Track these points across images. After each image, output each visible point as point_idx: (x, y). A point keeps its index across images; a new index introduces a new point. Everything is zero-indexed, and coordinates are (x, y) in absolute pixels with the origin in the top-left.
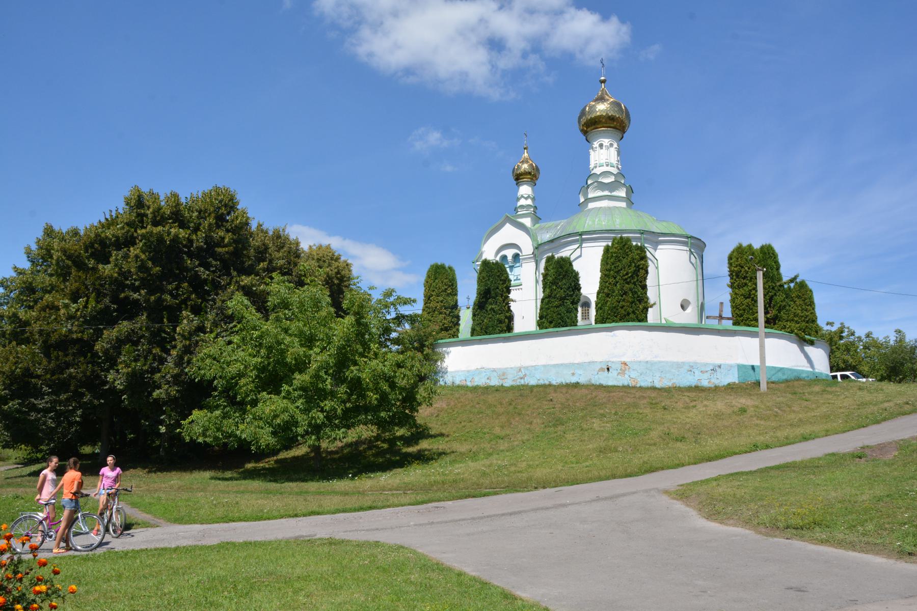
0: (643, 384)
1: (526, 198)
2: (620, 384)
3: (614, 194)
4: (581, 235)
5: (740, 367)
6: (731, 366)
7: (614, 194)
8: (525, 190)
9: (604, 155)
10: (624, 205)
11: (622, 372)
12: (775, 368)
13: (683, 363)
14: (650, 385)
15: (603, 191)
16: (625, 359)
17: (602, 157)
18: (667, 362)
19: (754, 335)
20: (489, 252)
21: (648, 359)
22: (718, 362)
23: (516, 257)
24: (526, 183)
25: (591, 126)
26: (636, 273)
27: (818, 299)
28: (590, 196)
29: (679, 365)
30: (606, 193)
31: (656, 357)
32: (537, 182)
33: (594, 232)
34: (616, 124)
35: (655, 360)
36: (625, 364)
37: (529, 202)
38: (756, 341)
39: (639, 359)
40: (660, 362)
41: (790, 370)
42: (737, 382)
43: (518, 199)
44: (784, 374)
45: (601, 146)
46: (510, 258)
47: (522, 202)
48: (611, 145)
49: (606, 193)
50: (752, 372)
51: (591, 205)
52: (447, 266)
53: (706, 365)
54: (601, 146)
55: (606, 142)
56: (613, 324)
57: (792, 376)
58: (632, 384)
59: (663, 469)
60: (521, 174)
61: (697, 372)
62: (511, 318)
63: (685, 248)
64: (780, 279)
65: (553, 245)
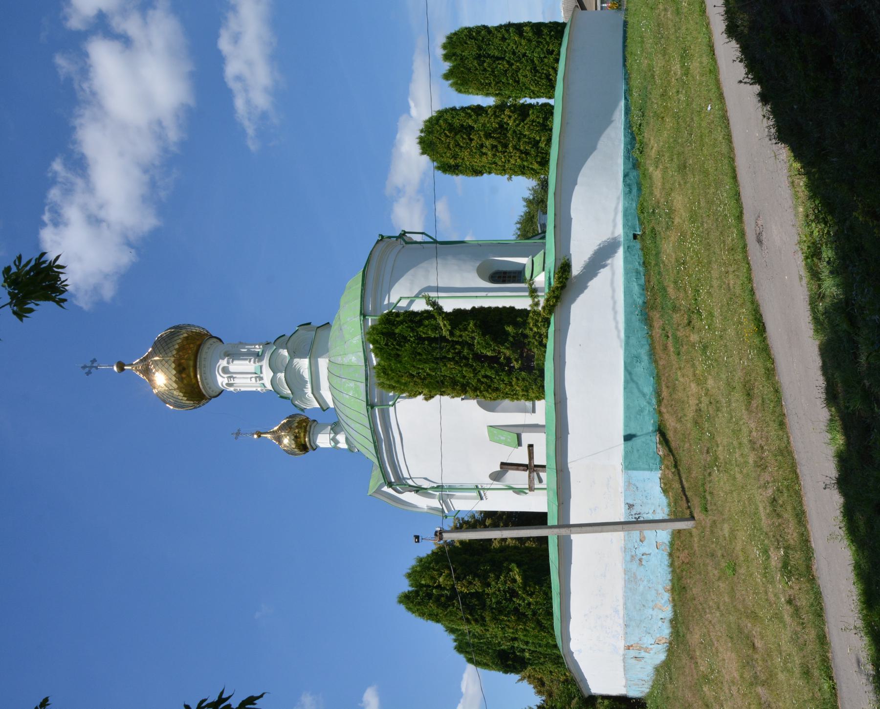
3: (306, 375)
5: (630, 464)
6: (629, 484)
7: (306, 375)
12: (626, 382)
13: (626, 572)
18: (626, 598)
19: (565, 547)
26: (471, 37)
27: (470, 21)
29: (631, 580)
30: (308, 390)
31: (617, 611)
35: (621, 613)
38: (578, 540)
40: (626, 607)
41: (627, 344)
42: (659, 474)
44: (637, 358)
48: (225, 370)
49: (308, 390)
50: (636, 442)
57: (641, 330)
59: (752, 292)
61: (643, 549)
62: (556, 24)
63: (391, 409)
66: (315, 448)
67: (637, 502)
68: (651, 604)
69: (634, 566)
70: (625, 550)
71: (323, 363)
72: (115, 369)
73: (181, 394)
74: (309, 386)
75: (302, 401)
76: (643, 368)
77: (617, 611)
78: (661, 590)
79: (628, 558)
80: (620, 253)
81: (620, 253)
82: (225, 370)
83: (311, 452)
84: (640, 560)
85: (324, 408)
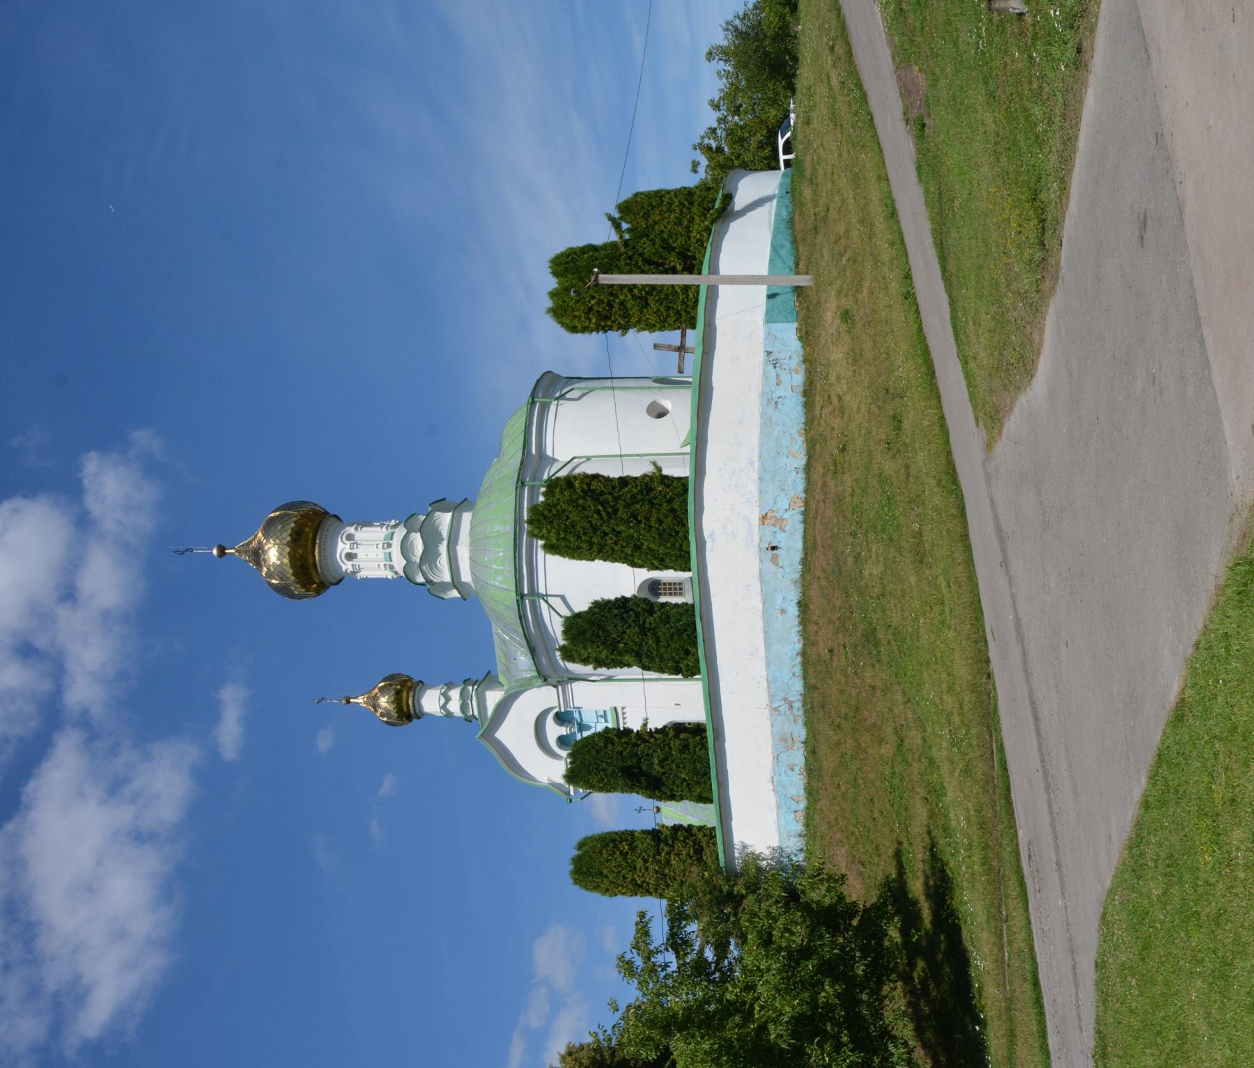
1: (448, 699)
2: (800, 527)
3: (445, 532)
5: (770, 318)
6: (768, 335)
7: (445, 532)
8: (430, 702)
11: (779, 523)
13: (762, 416)
14: (802, 475)
16: (755, 519)
18: (761, 445)
21: (755, 477)
22: (761, 357)
23: (561, 718)
29: (767, 423)
30: (443, 548)
31: (751, 463)
32: (416, 678)
35: (756, 464)
37: (455, 694)
39: (756, 494)
40: (761, 457)
42: (796, 325)
44: (782, 246)
45: (350, 557)
46: (563, 731)
47: (455, 707)
48: (350, 537)
49: (443, 548)
50: (779, 299)
51: (466, 577)
53: (765, 377)
54: (350, 557)
55: (342, 547)
56: (692, 538)
57: (787, 233)
59: (949, 453)
61: (780, 392)
63: (553, 407)
64: (613, 245)
65: (540, 650)
66: (419, 715)
67: (775, 350)
68: (785, 451)
69: (770, 409)
70: (763, 394)
71: (467, 517)
72: (215, 552)
73: (291, 571)
74: (445, 543)
75: (431, 568)
76: (787, 250)
77: (751, 463)
78: (796, 435)
79: (765, 402)
80: (775, 201)
81: (775, 201)
82: (350, 537)
83: (415, 721)
84: (776, 403)
85: (456, 583)
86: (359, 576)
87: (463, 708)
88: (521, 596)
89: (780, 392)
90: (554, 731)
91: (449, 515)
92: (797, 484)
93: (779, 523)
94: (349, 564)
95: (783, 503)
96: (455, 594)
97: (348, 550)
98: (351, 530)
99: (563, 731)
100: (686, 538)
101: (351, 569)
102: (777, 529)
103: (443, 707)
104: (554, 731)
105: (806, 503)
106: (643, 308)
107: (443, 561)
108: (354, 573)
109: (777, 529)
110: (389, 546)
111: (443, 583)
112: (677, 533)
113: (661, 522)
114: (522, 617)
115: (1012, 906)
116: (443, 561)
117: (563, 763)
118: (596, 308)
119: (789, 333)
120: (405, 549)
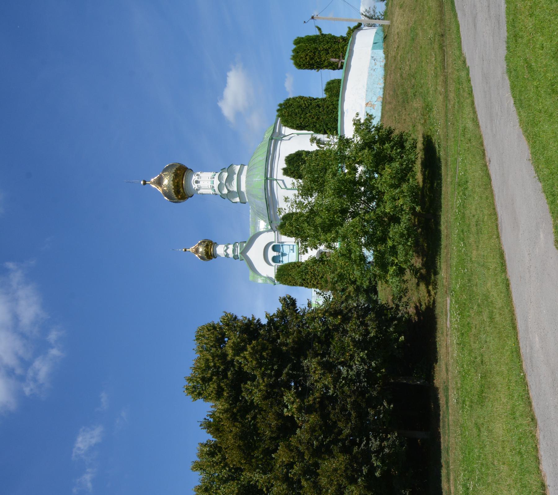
0: (382, 93)
1: (228, 248)
2: (380, 108)
4: (267, 178)
5: (373, 48)
6: (372, 53)
7: (237, 172)
8: (220, 250)
9: (204, 182)
10: (246, 168)
11: (373, 106)
14: (382, 90)
15: (233, 180)
16: (364, 105)
17: (206, 183)
20: (270, 271)
21: (365, 91)
22: (370, 58)
23: (275, 248)
24: (215, 250)
25: (180, 192)
28: (235, 189)
29: (370, 75)
30: (235, 177)
32: (214, 242)
33: (266, 169)
34: (181, 173)
35: (366, 87)
36: (367, 104)
37: (231, 247)
39: (365, 96)
40: (367, 84)
43: (227, 255)
45: (197, 182)
46: (275, 254)
47: (230, 251)
48: (198, 175)
49: (235, 177)
50: (377, 44)
51: (243, 188)
52: (294, 47)
53: (371, 63)
54: (197, 182)
55: (195, 178)
56: (339, 113)
58: (381, 99)
60: (207, 253)
61: (376, 67)
64: (317, 36)
65: (271, 206)
69: (372, 72)
72: (142, 182)
86: (199, 192)
87: (234, 251)
88: (267, 179)
89: (376, 67)
90: (271, 254)
91: (239, 166)
92: (380, 93)
93: (373, 106)
94: (196, 185)
95: (375, 99)
96: (237, 200)
97: (197, 179)
98: (199, 173)
99: (275, 254)
100: (337, 113)
101: (197, 188)
102: (372, 108)
103: (225, 251)
104: (271, 254)
105: (383, 98)
106: (327, 54)
107: (235, 183)
108: (197, 190)
109: (372, 108)
110: (214, 178)
111: (233, 192)
112: (334, 112)
113: (328, 107)
114: (266, 189)
115: (448, 16)
116: (235, 183)
117: (274, 267)
118: (309, 54)
119: (380, 54)
120: (220, 178)
